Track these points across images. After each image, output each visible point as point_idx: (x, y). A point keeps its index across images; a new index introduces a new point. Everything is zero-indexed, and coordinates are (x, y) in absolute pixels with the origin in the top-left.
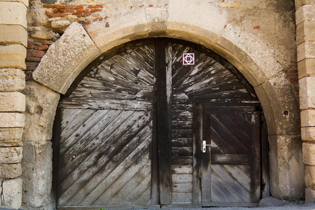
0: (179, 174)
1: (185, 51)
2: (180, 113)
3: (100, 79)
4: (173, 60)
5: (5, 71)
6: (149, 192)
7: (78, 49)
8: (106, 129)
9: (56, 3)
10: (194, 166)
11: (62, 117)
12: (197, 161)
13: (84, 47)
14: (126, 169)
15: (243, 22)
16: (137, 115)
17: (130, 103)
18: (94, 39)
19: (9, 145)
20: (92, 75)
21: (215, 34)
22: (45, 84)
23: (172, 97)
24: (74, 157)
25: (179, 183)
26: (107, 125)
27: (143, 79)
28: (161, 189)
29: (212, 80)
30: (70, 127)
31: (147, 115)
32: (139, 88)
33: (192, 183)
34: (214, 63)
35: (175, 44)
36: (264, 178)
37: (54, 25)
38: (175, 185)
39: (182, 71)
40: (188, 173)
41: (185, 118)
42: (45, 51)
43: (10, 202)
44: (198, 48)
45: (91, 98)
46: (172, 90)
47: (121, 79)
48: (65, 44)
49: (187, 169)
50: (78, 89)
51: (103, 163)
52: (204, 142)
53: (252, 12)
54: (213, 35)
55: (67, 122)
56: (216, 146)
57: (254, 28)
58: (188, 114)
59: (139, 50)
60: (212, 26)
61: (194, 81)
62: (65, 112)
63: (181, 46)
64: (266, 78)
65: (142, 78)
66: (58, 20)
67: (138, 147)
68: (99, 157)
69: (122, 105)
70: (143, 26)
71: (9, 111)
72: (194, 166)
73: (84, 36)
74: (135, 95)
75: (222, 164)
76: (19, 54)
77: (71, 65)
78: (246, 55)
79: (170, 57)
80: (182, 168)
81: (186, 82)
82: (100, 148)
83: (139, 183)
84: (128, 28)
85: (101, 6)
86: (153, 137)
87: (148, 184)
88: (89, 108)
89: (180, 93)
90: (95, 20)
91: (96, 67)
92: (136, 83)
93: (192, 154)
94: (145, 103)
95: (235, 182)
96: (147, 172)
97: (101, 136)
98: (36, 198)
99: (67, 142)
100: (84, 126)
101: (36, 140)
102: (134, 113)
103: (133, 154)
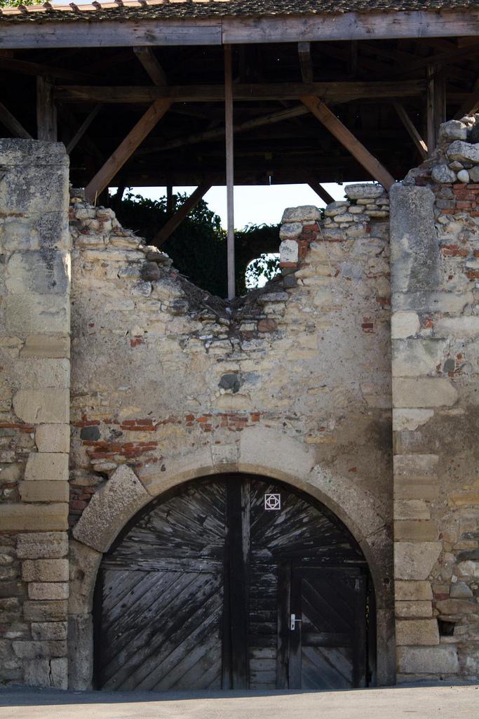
0: (259, 659)
1: (268, 491)
2: (261, 576)
3: (154, 530)
4: (251, 503)
5: (50, 535)
6: (219, 683)
7: (127, 499)
8: (161, 597)
9: (99, 441)
10: (279, 648)
11: (104, 582)
12: (283, 641)
13: (135, 497)
14: (189, 651)
15: (336, 462)
16: (203, 578)
17: (193, 562)
18: (147, 487)
19: (57, 620)
20: (142, 524)
21: (298, 479)
22: (88, 544)
23: (250, 554)
24: (120, 634)
25: (258, 671)
26: (163, 592)
27: (211, 530)
28: (235, 679)
29: (305, 532)
30: (115, 595)
31: (216, 579)
32: (205, 542)
33: (276, 671)
34: (307, 508)
35: (254, 481)
36: (370, 664)
37: (97, 468)
38: (254, 673)
39: (264, 518)
40: (271, 657)
41: (268, 584)
42: (88, 501)
43: (60, 683)
44: (284, 488)
45: (142, 556)
46: (251, 544)
47: (181, 530)
48: (112, 493)
49: (269, 653)
50: (124, 544)
51: (159, 643)
52: (293, 616)
53: (345, 450)
54: (298, 480)
55: (111, 588)
56: (308, 621)
57: (349, 471)
58: (272, 577)
59: (204, 491)
60: (296, 469)
61: (280, 533)
62: (107, 574)
63: (262, 483)
64: (363, 536)
65: (210, 528)
66: (102, 463)
67: (205, 622)
68: (152, 635)
69: (183, 565)
70: (209, 468)
71: (55, 580)
72: (279, 648)
73: (135, 482)
74: (200, 551)
75: (315, 645)
76: (62, 511)
77: (119, 519)
78: (338, 506)
79: (247, 500)
80: (263, 651)
81: (268, 533)
82: (153, 624)
83: (206, 671)
84: (189, 471)
85: (155, 443)
86: (222, 609)
87: (217, 672)
88: (138, 570)
89: (261, 549)
90: (147, 462)
91: (148, 515)
92: (202, 535)
93: (277, 633)
94: (213, 562)
95: (334, 670)
96: (216, 655)
97: (154, 607)
98: (80, 683)
99: (111, 614)
100: (132, 593)
101: (78, 612)
102: (200, 575)
103: (197, 631)
